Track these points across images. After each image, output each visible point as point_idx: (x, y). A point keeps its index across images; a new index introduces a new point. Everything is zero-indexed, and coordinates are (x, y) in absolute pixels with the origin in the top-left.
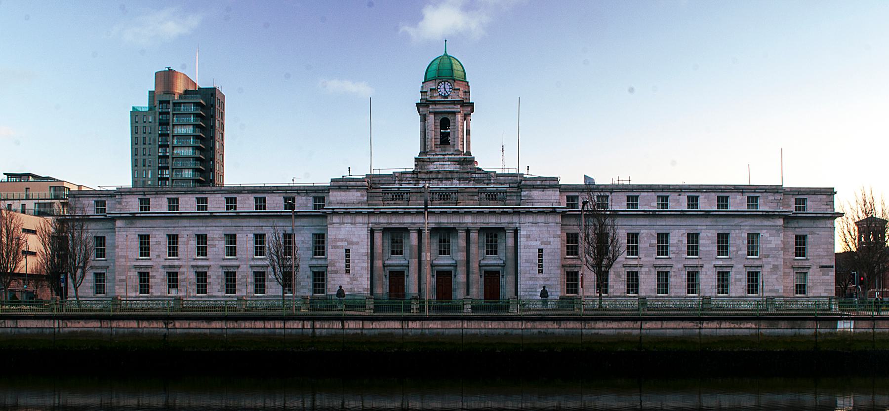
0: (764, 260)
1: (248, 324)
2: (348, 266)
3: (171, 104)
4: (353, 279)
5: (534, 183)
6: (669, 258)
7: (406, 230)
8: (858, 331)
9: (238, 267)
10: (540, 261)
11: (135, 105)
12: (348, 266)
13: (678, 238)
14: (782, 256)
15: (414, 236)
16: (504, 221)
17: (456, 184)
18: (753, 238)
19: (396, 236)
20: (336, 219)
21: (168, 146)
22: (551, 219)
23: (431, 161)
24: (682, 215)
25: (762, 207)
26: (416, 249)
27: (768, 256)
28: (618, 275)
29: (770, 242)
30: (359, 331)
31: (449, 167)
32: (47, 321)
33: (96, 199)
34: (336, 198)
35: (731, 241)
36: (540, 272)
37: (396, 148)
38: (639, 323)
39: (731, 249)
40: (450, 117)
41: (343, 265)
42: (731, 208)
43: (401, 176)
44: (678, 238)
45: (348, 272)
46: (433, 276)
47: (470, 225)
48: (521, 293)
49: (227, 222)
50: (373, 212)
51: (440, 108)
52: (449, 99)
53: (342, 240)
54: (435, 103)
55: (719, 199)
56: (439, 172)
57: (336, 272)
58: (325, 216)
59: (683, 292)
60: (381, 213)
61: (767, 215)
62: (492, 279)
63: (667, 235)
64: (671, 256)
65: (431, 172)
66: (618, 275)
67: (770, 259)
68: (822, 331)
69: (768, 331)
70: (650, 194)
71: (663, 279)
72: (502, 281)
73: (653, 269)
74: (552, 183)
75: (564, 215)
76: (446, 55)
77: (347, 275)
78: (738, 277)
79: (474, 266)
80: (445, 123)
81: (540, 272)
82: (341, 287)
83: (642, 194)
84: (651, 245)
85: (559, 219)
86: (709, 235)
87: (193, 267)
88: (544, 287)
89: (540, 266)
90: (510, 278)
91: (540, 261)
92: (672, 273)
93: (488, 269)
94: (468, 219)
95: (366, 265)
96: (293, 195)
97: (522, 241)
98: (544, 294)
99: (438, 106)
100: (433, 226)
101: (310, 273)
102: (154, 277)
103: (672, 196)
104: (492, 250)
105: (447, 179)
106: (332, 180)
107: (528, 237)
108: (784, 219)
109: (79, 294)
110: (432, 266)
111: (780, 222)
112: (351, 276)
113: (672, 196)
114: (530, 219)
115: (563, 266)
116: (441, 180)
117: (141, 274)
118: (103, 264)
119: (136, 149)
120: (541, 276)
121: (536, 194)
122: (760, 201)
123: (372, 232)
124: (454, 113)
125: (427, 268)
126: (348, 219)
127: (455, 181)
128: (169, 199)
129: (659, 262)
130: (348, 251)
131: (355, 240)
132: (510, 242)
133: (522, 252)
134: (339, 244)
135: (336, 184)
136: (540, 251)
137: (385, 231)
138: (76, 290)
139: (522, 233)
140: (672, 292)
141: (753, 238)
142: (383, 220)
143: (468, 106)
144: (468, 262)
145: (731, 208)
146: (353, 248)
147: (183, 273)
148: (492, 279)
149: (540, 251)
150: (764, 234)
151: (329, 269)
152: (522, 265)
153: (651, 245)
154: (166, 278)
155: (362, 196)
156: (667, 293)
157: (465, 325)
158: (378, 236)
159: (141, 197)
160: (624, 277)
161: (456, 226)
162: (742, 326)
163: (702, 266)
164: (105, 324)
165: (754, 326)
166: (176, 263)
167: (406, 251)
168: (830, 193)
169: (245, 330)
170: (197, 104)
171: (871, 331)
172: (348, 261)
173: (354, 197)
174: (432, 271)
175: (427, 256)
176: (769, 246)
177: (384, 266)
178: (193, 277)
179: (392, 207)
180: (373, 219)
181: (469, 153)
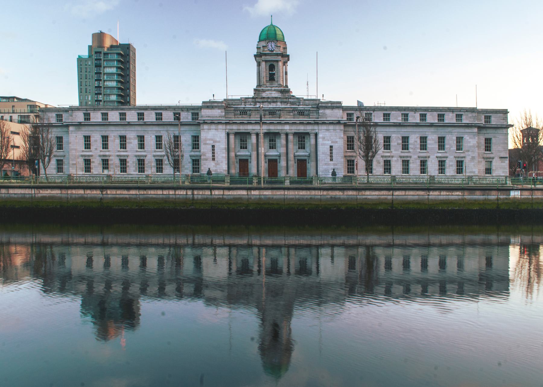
0: (466, 153)
1: (152, 192)
2: (213, 156)
4: (217, 164)
5: (327, 105)
6: (409, 152)
8: (523, 197)
10: (331, 153)
12: (213, 156)
13: (414, 140)
14: (477, 151)
15: (254, 137)
16: (309, 128)
17: (279, 105)
18: (459, 140)
19: (243, 137)
20: (206, 127)
21: (101, 80)
22: (337, 127)
23: (264, 91)
24: (417, 125)
25: (465, 121)
27: (468, 151)
29: (470, 142)
30: (221, 197)
31: (275, 94)
34: (205, 113)
36: (331, 160)
37: (241, 82)
38: (391, 192)
40: (275, 64)
42: (446, 121)
43: (245, 100)
44: (414, 140)
45: (214, 159)
46: (266, 162)
47: (288, 131)
48: (320, 173)
49: (139, 128)
51: (269, 58)
52: (274, 52)
53: (210, 140)
54: (265, 55)
55: (384, 115)
56: (268, 98)
57: (206, 160)
58: (199, 124)
60: (234, 123)
61: (468, 126)
62: (302, 164)
64: (410, 150)
65: (264, 98)
66: (379, 162)
67: (470, 153)
68: (502, 197)
69: (469, 197)
70: (397, 112)
73: (399, 159)
74: (338, 105)
75: (345, 125)
76: (272, 25)
79: (291, 156)
80: (272, 68)
81: (331, 160)
83: (393, 112)
84: (398, 144)
86: (433, 138)
87: (118, 156)
88: (334, 170)
89: (331, 156)
91: (331, 153)
92: (411, 161)
93: (299, 158)
94: (287, 127)
95: (225, 155)
96: (179, 111)
97: (320, 141)
98: (334, 174)
99: (267, 57)
100: (266, 131)
101: (190, 160)
103: (411, 114)
104: (302, 147)
105: (274, 102)
106: (204, 102)
107: (323, 138)
109: (47, 173)
110: (265, 156)
112: (216, 162)
113: (411, 114)
114: (324, 127)
115: (345, 156)
116: (270, 102)
117: (85, 160)
118: (62, 154)
119: (81, 82)
120: (332, 162)
122: (464, 117)
123: (228, 135)
125: (262, 158)
126: (213, 126)
127: (279, 104)
128: (103, 114)
130: (213, 146)
131: (218, 140)
132: (313, 141)
133: (321, 149)
134: (208, 142)
136: (331, 147)
139: (320, 136)
141: (459, 140)
142: (235, 127)
145: (446, 121)
146: (217, 145)
147: (112, 160)
148: (302, 164)
149: (331, 147)
150: (466, 137)
151: (202, 157)
152: (320, 156)
153: (398, 144)
154: (101, 163)
155: (222, 112)
157: (286, 193)
158: (232, 137)
159: (85, 112)
160: (382, 163)
161: (280, 131)
162: (453, 194)
163: (429, 157)
164: (64, 191)
165: (460, 194)
166: (107, 153)
167: (249, 147)
168: (505, 112)
169: (151, 196)
170: (119, 54)
171: (530, 197)
172: (213, 153)
173: (217, 113)
175: (262, 150)
176: (469, 145)
177: (236, 156)
178: (118, 162)
179: (240, 119)
180: (229, 127)
181: (287, 86)
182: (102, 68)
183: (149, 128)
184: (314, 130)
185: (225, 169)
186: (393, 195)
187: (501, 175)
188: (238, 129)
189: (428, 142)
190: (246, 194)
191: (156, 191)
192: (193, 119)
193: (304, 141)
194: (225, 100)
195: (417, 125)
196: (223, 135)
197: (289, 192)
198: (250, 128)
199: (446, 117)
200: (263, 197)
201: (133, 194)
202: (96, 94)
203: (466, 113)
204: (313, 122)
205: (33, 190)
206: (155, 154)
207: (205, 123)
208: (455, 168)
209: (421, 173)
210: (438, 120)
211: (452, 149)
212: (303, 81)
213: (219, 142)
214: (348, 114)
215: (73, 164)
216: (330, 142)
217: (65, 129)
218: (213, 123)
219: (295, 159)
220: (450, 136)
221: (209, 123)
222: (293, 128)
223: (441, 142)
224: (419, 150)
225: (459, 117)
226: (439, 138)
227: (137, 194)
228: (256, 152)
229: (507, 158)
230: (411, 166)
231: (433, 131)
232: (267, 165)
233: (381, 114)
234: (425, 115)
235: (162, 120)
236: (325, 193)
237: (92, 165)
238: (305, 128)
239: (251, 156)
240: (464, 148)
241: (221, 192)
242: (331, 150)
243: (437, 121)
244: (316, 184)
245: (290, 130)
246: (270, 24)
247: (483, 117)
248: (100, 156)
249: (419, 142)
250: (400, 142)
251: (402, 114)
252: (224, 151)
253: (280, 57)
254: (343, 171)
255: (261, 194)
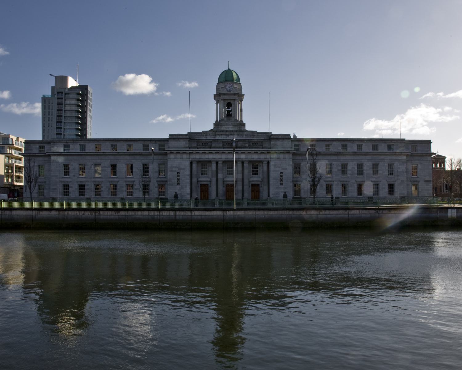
0: (396, 178)
1: (140, 213)
2: (178, 181)
3: (64, 94)
5: (278, 137)
6: (348, 177)
7: (209, 162)
9: (118, 182)
10: (282, 179)
11: (44, 94)
12: (178, 181)
14: (406, 175)
15: (214, 165)
16: (262, 157)
18: (391, 166)
19: (204, 164)
20: (172, 156)
22: (287, 156)
24: (355, 154)
26: (219, 171)
28: (322, 186)
29: (399, 168)
31: (231, 128)
32: (283, 211)
33: (40, 145)
34: (173, 145)
35: (380, 168)
36: (281, 184)
37: (202, 118)
38: (348, 211)
39: (380, 172)
40: (232, 102)
41: (176, 180)
46: (224, 187)
47: (244, 159)
48: (271, 196)
49: (112, 157)
50: (192, 153)
51: (226, 97)
52: (232, 92)
54: (224, 94)
55: (373, 146)
56: (227, 131)
57: (172, 185)
58: (166, 154)
59: (355, 194)
60: (196, 153)
62: (255, 187)
63: (347, 165)
65: (223, 131)
71: (391, 188)
72: (261, 189)
73: (339, 183)
74: (287, 137)
75: (294, 154)
76: (229, 69)
77: (178, 186)
78: (383, 186)
79: (246, 181)
80: (229, 105)
82: (176, 193)
84: (338, 170)
85: (291, 156)
86: (369, 165)
87: (93, 182)
88: (285, 192)
89: (281, 181)
90: (266, 188)
91: (282, 179)
93: (228, 183)
95: (188, 181)
97: (272, 168)
98: (285, 196)
100: (224, 160)
101: (157, 185)
102: (72, 187)
104: (256, 173)
106: (170, 135)
107: (275, 166)
108: (406, 156)
109: (32, 197)
110: (224, 181)
111: (404, 158)
115: (293, 181)
117: (64, 186)
119: (45, 118)
120: (282, 186)
121: (279, 143)
123: (191, 163)
124: (234, 100)
125: (220, 182)
126: (178, 156)
128: (80, 145)
129: (342, 179)
130: (178, 173)
132: (265, 168)
133: (272, 174)
134: (174, 169)
135: (172, 137)
136: (281, 173)
137: (198, 162)
138: (31, 194)
139: (272, 164)
140: (350, 194)
141: (391, 166)
143: (241, 96)
144: (243, 179)
145: (379, 151)
148: (255, 187)
150: (396, 164)
151: (168, 183)
152: (271, 182)
153: (338, 170)
154: (78, 187)
155: (186, 143)
156: (378, 195)
157: (257, 213)
158: (194, 165)
159: (65, 144)
160: (325, 187)
167: (209, 173)
168: (429, 142)
169: (138, 216)
174: (223, 184)
175: (220, 176)
177: (198, 181)
178: (93, 188)
180: (192, 156)
181: (242, 121)
182: (63, 106)
183: (122, 157)
184: (266, 158)
185: (188, 192)
186: (349, 214)
187: (426, 196)
188: (226, 158)
189: (364, 168)
190: (222, 214)
191: (142, 212)
192: (160, 149)
193: (207, 168)
194: (188, 133)
195: (355, 154)
196: (187, 164)
197: (259, 212)
198: (211, 156)
199: (379, 147)
200: (236, 217)
201: (122, 215)
202: (57, 128)
203: (396, 143)
204: (266, 152)
205: (34, 211)
206: (62, 180)
207: (171, 153)
208: (387, 190)
209: (358, 195)
210: (373, 149)
211: (384, 174)
212: (256, 119)
213: (184, 169)
214: (295, 145)
215: (53, 189)
216: (280, 169)
217: (46, 159)
218: (179, 153)
219: (249, 183)
220: (383, 163)
221: (181, 153)
222: (203, 157)
223: (375, 167)
224: (356, 176)
225: (360, 147)
226: (373, 164)
227: (126, 215)
228: (215, 178)
229: (431, 181)
230: (350, 189)
231: (229, 159)
232: (225, 189)
233: (370, 144)
234: (361, 145)
235: (85, 151)
236: (291, 213)
237: (70, 189)
238: (220, 157)
239: (211, 182)
240: (395, 174)
241: (357, 212)
242: (281, 176)
243: (371, 151)
244: (270, 206)
245: (245, 158)
246: (227, 69)
247: (410, 146)
248: (78, 182)
249: (356, 168)
250: (340, 168)
251: (326, 145)
252: (188, 177)
253: (237, 96)
254: (292, 194)
255: (235, 214)
